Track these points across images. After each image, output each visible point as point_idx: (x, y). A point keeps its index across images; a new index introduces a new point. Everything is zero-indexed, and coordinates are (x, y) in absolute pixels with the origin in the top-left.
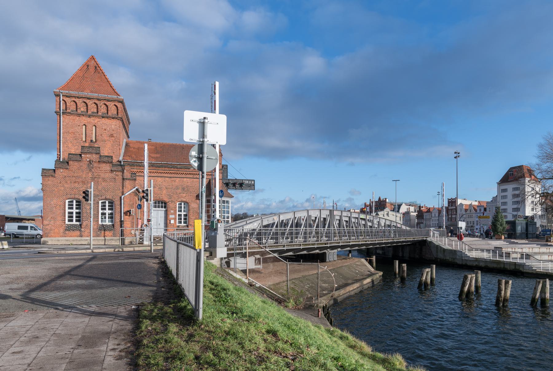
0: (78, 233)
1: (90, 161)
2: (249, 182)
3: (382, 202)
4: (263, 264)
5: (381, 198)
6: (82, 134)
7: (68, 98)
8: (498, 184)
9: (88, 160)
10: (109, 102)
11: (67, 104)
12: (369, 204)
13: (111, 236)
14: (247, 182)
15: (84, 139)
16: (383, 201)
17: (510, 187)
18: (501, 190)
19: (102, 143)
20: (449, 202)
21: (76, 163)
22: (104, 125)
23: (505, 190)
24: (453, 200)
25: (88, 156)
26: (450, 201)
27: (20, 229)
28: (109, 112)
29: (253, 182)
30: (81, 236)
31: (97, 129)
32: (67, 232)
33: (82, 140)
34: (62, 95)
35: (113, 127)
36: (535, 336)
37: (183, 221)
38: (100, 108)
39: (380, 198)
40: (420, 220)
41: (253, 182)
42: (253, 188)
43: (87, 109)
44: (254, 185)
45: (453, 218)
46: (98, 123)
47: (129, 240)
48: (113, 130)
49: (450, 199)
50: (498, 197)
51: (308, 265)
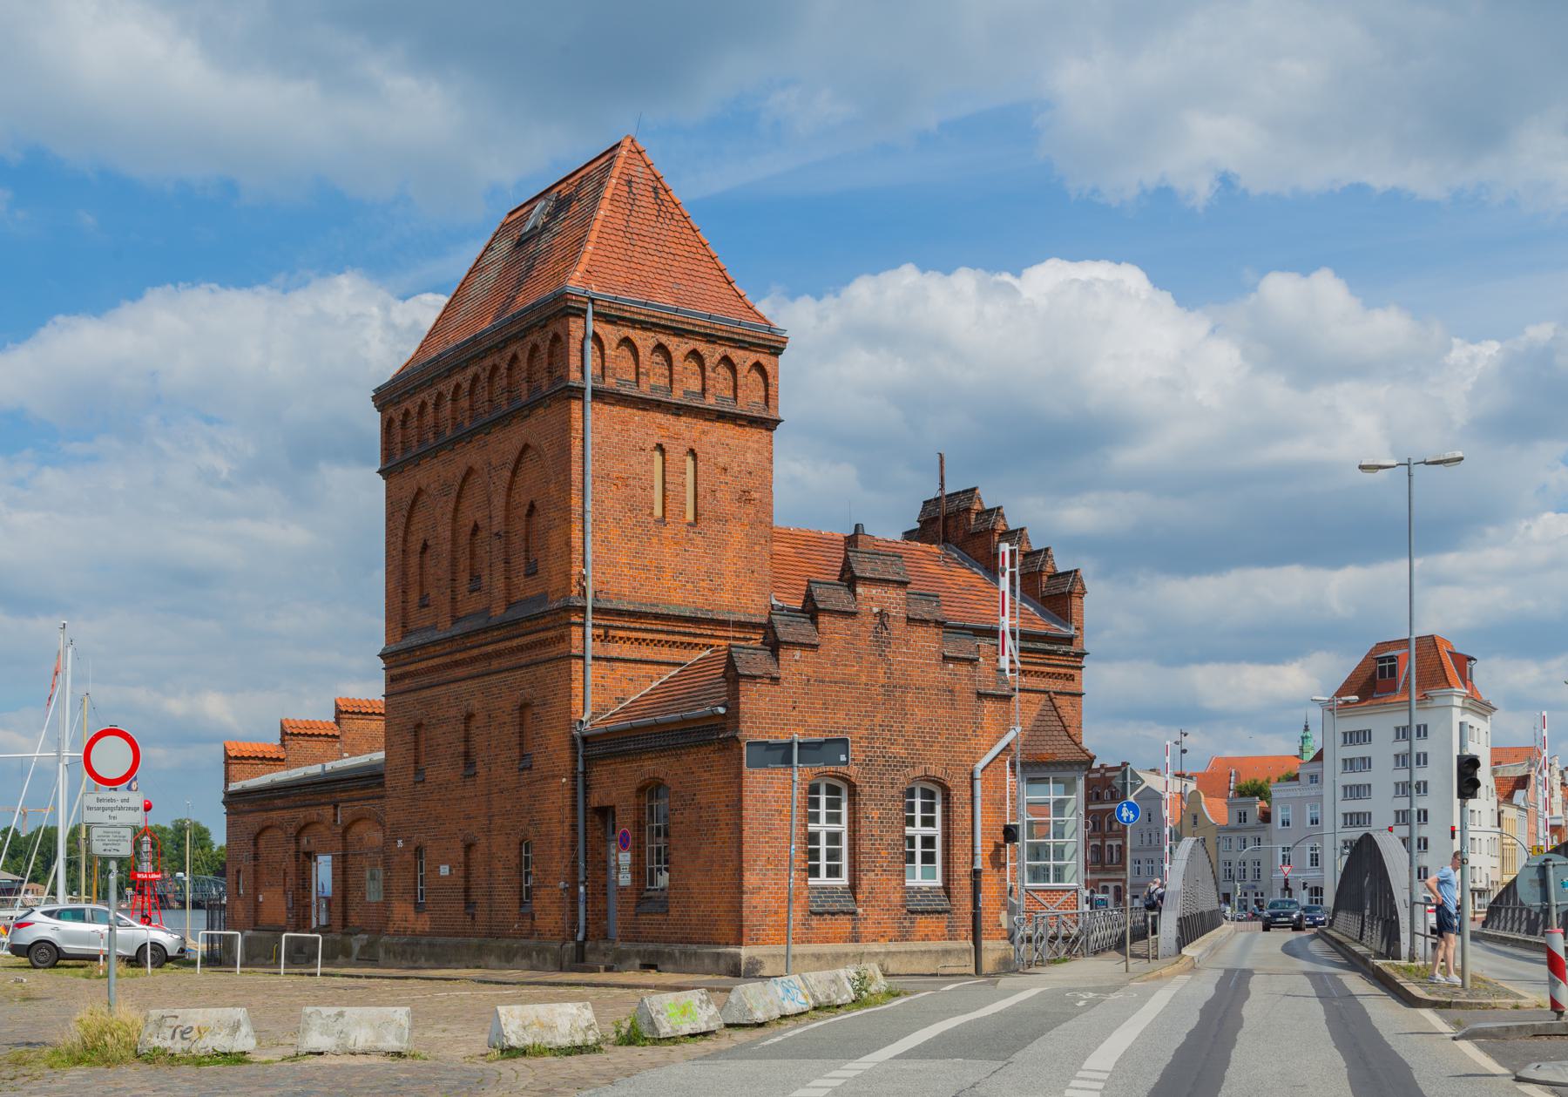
0: (844, 923)
1: (881, 613)
4: (194, 957)
6: (652, 487)
7: (609, 328)
9: (876, 610)
10: (740, 352)
11: (607, 352)
13: (942, 938)
15: (658, 512)
17: (1382, 723)
18: (1340, 739)
19: (716, 527)
21: (841, 623)
22: (721, 451)
23: (1363, 737)
24: (1108, 774)
25: (874, 591)
26: (1098, 775)
28: (740, 394)
30: (855, 938)
31: (700, 464)
32: (815, 922)
33: (651, 514)
34: (595, 314)
35: (750, 458)
37: (823, 847)
38: (713, 375)
43: (671, 381)
46: (704, 438)
47: (997, 955)
48: (750, 473)
51: (609, 982)
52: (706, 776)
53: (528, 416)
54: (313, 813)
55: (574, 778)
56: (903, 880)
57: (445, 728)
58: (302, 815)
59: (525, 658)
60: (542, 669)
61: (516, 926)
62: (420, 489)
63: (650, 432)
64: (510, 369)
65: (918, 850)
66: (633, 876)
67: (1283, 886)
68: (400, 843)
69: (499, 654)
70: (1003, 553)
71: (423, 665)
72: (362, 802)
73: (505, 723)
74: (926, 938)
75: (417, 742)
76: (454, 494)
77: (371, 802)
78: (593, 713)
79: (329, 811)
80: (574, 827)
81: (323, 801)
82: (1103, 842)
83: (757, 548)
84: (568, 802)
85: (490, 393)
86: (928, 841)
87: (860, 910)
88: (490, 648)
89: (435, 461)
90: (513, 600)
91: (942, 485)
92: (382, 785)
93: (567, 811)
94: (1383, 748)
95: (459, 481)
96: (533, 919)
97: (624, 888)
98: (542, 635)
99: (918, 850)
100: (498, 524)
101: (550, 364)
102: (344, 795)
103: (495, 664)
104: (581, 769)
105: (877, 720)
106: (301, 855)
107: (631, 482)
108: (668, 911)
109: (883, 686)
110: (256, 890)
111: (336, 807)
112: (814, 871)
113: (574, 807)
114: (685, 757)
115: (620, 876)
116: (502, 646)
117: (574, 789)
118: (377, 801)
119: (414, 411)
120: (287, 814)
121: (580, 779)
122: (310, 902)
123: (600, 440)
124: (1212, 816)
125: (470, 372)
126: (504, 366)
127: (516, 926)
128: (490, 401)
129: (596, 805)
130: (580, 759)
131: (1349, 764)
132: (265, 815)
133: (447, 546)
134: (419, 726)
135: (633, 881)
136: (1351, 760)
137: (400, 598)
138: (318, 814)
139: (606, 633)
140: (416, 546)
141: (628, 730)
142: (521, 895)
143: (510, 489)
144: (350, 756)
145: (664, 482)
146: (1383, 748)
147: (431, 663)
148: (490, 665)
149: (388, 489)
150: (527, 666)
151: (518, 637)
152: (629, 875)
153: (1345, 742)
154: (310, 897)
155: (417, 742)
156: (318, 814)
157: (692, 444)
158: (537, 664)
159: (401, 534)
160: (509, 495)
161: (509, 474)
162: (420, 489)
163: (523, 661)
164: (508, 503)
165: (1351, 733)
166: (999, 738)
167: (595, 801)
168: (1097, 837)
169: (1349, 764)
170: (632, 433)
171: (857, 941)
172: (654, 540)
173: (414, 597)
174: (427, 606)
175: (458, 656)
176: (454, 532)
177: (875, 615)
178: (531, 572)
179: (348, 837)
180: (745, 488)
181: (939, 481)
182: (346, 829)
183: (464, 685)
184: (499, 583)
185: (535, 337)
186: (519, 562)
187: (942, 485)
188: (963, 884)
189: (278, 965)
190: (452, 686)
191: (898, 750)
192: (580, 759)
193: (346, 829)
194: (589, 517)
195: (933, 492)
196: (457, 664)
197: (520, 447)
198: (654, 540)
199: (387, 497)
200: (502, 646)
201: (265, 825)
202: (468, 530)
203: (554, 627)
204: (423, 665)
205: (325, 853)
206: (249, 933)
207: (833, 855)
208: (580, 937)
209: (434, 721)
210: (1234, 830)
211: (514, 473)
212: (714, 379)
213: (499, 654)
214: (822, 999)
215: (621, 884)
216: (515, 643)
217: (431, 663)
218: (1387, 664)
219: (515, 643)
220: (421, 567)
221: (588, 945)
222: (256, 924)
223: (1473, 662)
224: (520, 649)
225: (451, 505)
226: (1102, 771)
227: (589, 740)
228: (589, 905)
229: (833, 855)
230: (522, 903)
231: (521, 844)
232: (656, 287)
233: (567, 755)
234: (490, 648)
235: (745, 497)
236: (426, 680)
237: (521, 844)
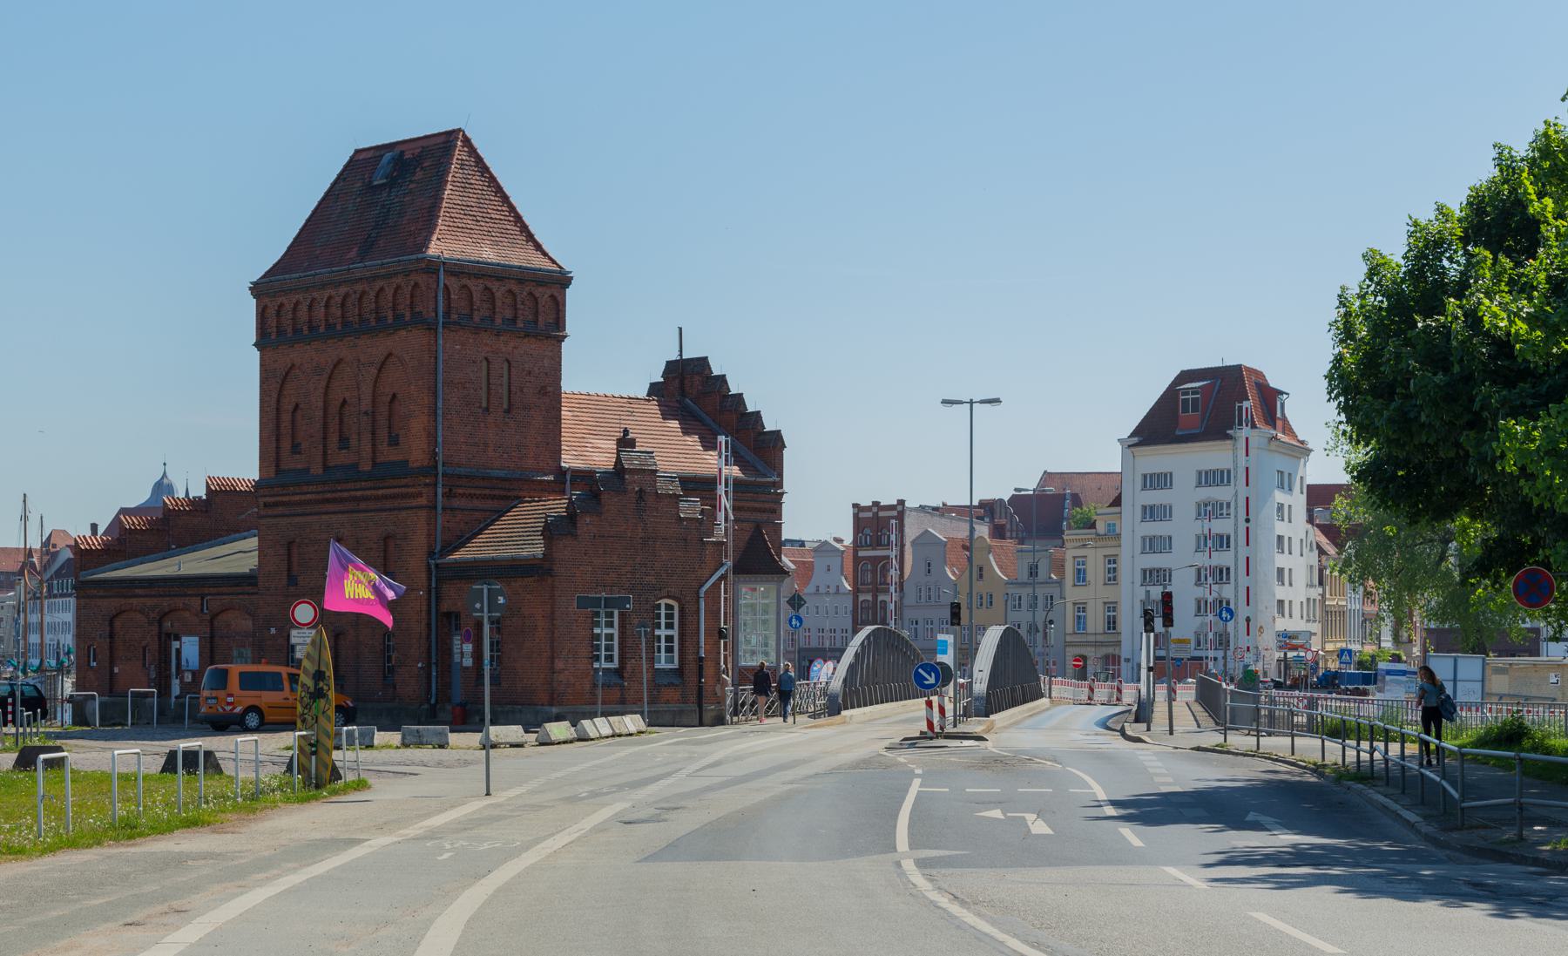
9: (637, 489)
24: (881, 514)
25: (636, 477)
26: (870, 514)
38: (522, 307)
52: (528, 596)
53: (393, 333)
54: (179, 602)
55: (429, 592)
56: (653, 664)
57: (316, 547)
58: (166, 603)
59: (388, 504)
60: (404, 513)
61: (380, 693)
62: (293, 365)
63: (480, 350)
64: (377, 296)
65: (663, 644)
66: (473, 660)
67: (1313, 631)
68: (273, 631)
69: (366, 499)
70: (720, 442)
71: (297, 498)
72: (231, 597)
73: (371, 549)
74: (668, 702)
75: (289, 555)
76: (326, 376)
77: (241, 597)
78: (442, 547)
79: (196, 602)
80: (429, 625)
81: (189, 593)
82: (875, 597)
83: (551, 426)
84: (424, 608)
85: (360, 310)
86: (669, 639)
87: (626, 684)
88: (359, 493)
89: (308, 347)
90: (378, 461)
91: (681, 351)
92: (255, 585)
93: (424, 614)
94: (1184, 497)
95: (331, 367)
96: (395, 688)
97: (467, 668)
98: (404, 490)
99: (663, 644)
100: (366, 404)
101: (412, 302)
102: (212, 590)
103: (363, 506)
104: (434, 585)
105: (638, 559)
106: (163, 636)
107: (467, 385)
108: (500, 684)
109: (641, 538)
110: (112, 664)
111: (202, 599)
112: (597, 658)
113: (429, 612)
114: (513, 584)
115: (464, 659)
116: (368, 493)
117: (429, 600)
118: (246, 597)
119: (289, 307)
120: (149, 602)
121: (433, 591)
122: (170, 674)
123: (447, 358)
124: (1000, 568)
125: (343, 290)
126: (372, 294)
127: (380, 693)
128: (360, 315)
129: (445, 610)
130: (433, 578)
131: (1150, 513)
132: (123, 601)
133: (320, 413)
134: (290, 543)
135: (474, 663)
136: (1152, 508)
137: (274, 445)
138: (184, 603)
139: (450, 490)
140: (288, 406)
141: (471, 562)
142: (384, 671)
143: (376, 382)
144: (177, 548)
145: (489, 384)
146: (1184, 497)
147: (303, 497)
148: (358, 505)
149: (261, 358)
150: (390, 510)
151: (382, 488)
152: (471, 659)
153: (1145, 486)
154: (170, 670)
155: (289, 555)
156: (184, 603)
157: (507, 356)
158: (399, 509)
159: (275, 396)
160: (375, 386)
161: (376, 371)
162: (293, 365)
163: (388, 506)
164: (374, 391)
165: (1151, 475)
166: (717, 570)
167: (445, 607)
168: (868, 591)
169: (1150, 513)
170: (469, 352)
171: (624, 704)
172: (482, 425)
173: (286, 445)
174: (299, 453)
175: (329, 495)
176: (326, 403)
177: (637, 492)
178: (394, 441)
179: (216, 623)
180: (542, 384)
181: (678, 349)
182: (214, 617)
183: (334, 518)
184: (367, 448)
185: (399, 280)
186: (383, 434)
187: (681, 351)
188: (692, 667)
189: (183, 723)
190: (323, 517)
191: (651, 579)
192: (433, 578)
193: (214, 617)
194: (440, 412)
195: (674, 356)
196: (327, 501)
197: (385, 354)
198: (482, 425)
199: (261, 365)
200: (368, 493)
201: (123, 608)
202: (338, 403)
203: (414, 485)
204: (297, 498)
205: (191, 634)
206: (105, 699)
207: (609, 648)
208: (433, 701)
209: (306, 541)
210: (1024, 584)
211: (380, 371)
212: (523, 310)
213: (366, 499)
214: (617, 731)
215: (464, 665)
216: (380, 492)
217: (303, 497)
218: (1190, 397)
219: (380, 492)
220: (293, 422)
221: (438, 706)
222: (111, 691)
223: (1285, 396)
224: (385, 497)
225: (324, 383)
226: (875, 509)
227: (440, 566)
228: (439, 679)
229: (609, 648)
230: (385, 678)
231: (384, 635)
232: (482, 245)
233: (424, 576)
234: (359, 493)
235: (543, 391)
236: (299, 510)
237: (384, 635)
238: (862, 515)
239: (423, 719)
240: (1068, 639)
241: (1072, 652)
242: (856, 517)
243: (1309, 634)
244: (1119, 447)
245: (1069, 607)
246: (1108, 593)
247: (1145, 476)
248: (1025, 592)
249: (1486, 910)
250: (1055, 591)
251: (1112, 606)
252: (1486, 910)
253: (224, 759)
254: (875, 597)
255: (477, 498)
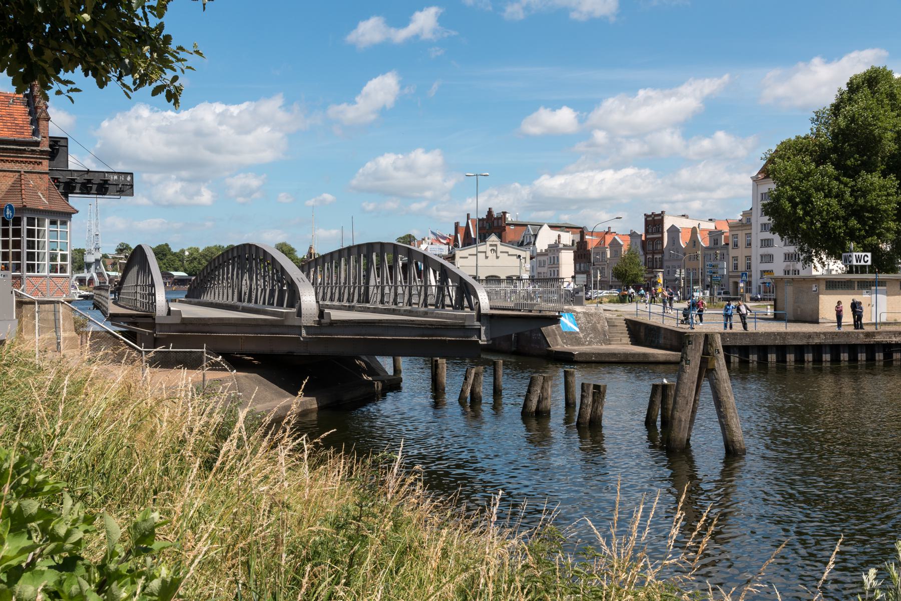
2: (119, 177)
3: (496, 222)
5: (493, 210)
8: (755, 180)
12: (465, 225)
14: (116, 177)
16: (498, 219)
20: (647, 222)
24: (656, 218)
26: (651, 219)
27: (8, 257)
29: (129, 178)
36: (626, 433)
39: (490, 212)
40: (582, 265)
41: (129, 178)
42: (62, 143)
44: (132, 186)
45: (656, 261)
49: (650, 216)
50: (754, 211)
82: (653, 256)
238: (648, 219)
239: (663, 332)
240: (730, 274)
241: (732, 280)
242: (646, 219)
243: (769, 257)
244: (751, 181)
245: (731, 259)
246: (746, 252)
247: (762, 194)
248: (712, 252)
249: (719, 403)
250: (725, 252)
251: (749, 258)
252: (719, 403)
253: (627, 344)
254: (653, 256)
255: (30, 114)
